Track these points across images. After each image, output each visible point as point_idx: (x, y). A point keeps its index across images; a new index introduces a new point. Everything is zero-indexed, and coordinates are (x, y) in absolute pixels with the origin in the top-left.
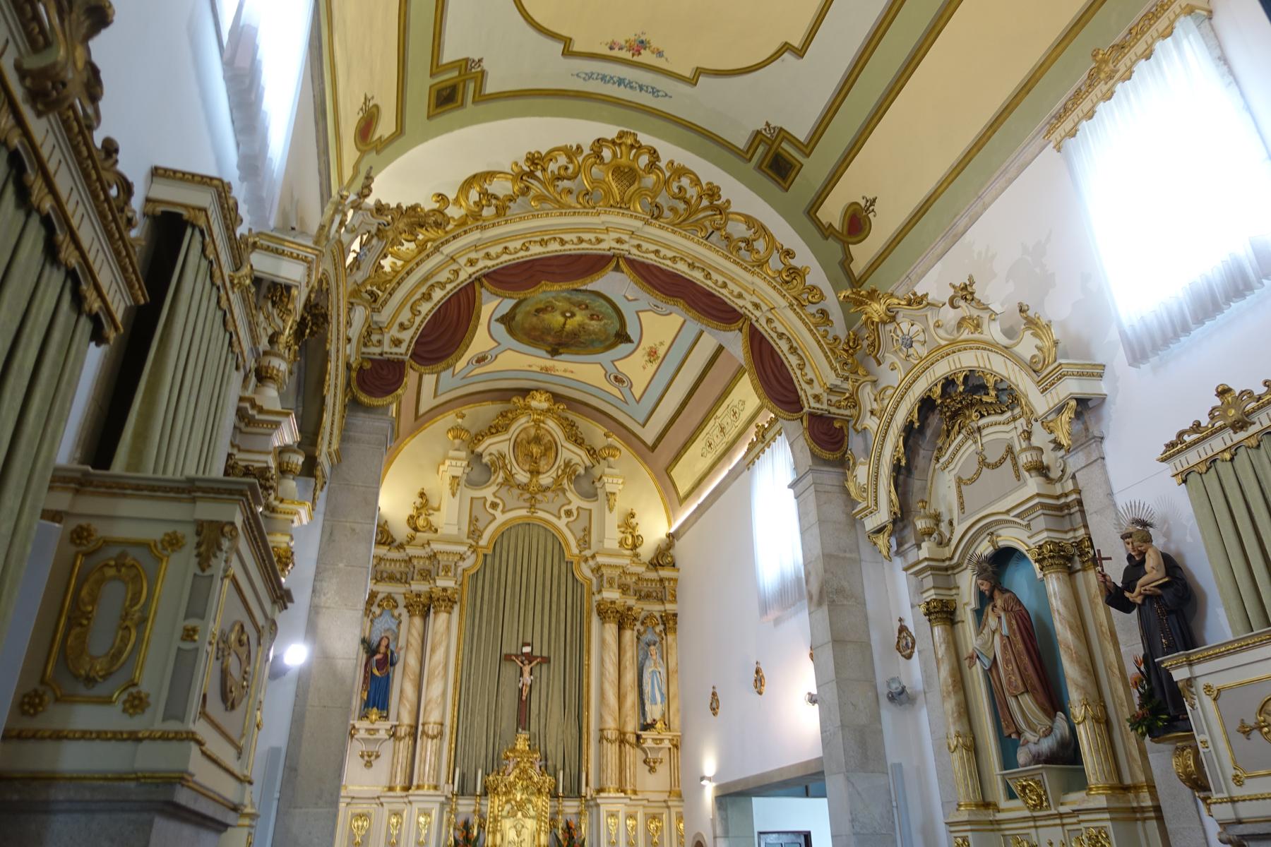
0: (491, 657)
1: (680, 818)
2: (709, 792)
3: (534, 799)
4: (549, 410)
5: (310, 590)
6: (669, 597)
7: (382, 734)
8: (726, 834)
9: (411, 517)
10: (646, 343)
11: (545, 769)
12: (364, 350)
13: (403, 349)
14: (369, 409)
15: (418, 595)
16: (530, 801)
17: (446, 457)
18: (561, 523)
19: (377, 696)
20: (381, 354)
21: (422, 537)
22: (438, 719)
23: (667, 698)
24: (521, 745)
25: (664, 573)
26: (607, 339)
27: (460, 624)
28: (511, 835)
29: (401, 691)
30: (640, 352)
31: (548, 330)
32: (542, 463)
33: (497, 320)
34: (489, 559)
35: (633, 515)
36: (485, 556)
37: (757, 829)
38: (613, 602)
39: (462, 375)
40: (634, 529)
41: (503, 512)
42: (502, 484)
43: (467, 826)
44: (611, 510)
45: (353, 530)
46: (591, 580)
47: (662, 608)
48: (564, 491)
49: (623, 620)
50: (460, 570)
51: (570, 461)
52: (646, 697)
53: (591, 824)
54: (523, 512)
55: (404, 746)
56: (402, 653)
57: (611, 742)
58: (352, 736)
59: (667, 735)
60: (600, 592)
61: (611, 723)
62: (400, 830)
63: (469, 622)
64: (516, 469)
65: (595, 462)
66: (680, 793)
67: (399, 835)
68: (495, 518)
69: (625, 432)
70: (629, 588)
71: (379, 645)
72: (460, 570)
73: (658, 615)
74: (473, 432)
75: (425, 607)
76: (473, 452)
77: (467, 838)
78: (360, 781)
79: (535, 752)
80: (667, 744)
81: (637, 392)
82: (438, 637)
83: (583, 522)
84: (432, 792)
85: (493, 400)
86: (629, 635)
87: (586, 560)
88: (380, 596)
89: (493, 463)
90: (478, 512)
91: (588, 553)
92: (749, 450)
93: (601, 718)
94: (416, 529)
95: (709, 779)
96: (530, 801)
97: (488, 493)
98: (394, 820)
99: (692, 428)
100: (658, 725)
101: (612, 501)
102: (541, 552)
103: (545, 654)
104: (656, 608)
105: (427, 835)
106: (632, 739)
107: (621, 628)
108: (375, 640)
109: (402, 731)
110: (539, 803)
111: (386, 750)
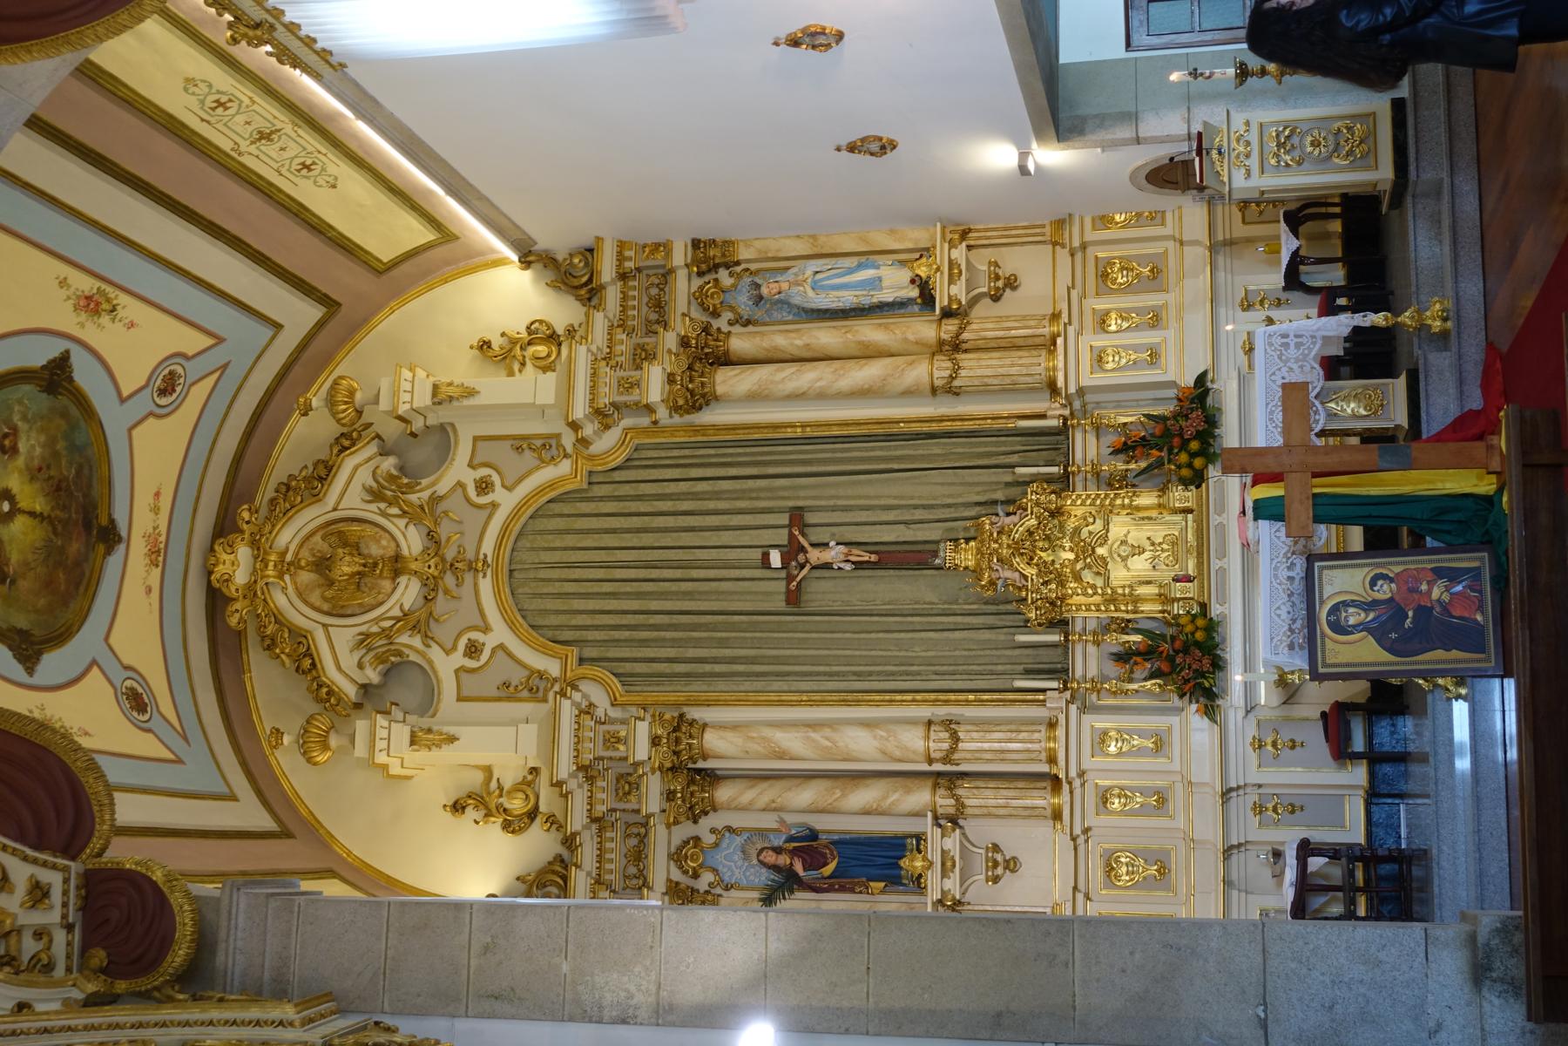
0: (793, 627)
1: (1104, 221)
2: (1051, 156)
3: (1071, 524)
4: (254, 544)
5: (622, 1029)
6: (659, 258)
7: (952, 843)
8: (1133, 117)
9: (507, 826)
10: (67, 320)
11: (1012, 505)
12: (60, 971)
13: (54, 879)
14: (204, 942)
15: (670, 796)
16: (1077, 531)
17: (370, 763)
18: (507, 501)
19: (877, 861)
20: (69, 928)
21: (547, 800)
22: (920, 731)
23: (868, 256)
24: (967, 557)
25: (607, 269)
26: (64, 415)
27: (726, 704)
28: (1140, 565)
29: (867, 812)
30: (90, 334)
31: (52, 554)
32: (375, 551)
33: (30, 671)
34: (590, 652)
35: (485, 345)
36: (581, 661)
37: (1119, 52)
38: (671, 379)
39: (177, 744)
40: (513, 342)
41: (486, 629)
42: (427, 638)
43: (1124, 657)
44: (471, 393)
45: (486, 949)
46: (626, 431)
47: (682, 275)
48: (435, 500)
49: (705, 355)
50: (615, 713)
51: (370, 491)
52: (866, 301)
53: (1118, 404)
54: (486, 585)
55: (975, 798)
56: (791, 819)
57: (957, 369)
58: (958, 903)
59: (942, 254)
60: (649, 409)
61: (919, 372)
62: (1133, 789)
63: (721, 685)
64: (391, 608)
65: (370, 433)
66: (1056, 223)
67: (1143, 791)
68: (501, 647)
69: (297, 370)
70: (642, 347)
71: (775, 868)
72: (615, 713)
73: (697, 282)
74: (313, 708)
75: (694, 780)
76: (358, 706)
77: (1147, 653)
78: (1043, 881)
79: (979, 527)
80: (959, 253)
81: (193, 341)
82: (754, 747)
83: (501, 454)
84: (1060, 732)
85: (240, 669)
86: (740, 343)
87: (584, 442)
88: (676, 875)
89: (380, 659)
90: (490, 686)
91: (568, 440)
92: (296, 63)
93: (909, 393)
94: (532, 815)
95: (1024, 156)
96: (1077, 531)
97: (446, 665)
98: (1116, 804)
99: (271, 212)
100: (923, 272)
101: (452, 391)
102: (570, 540)
103: (784, 519)
104: (683, 286)
105: (1141, 734)
106: (950, 326)
107: (726, 360)
108: (765, 876)
109: (945, 803)
110: (1079, 511)
111: (981, 831)
